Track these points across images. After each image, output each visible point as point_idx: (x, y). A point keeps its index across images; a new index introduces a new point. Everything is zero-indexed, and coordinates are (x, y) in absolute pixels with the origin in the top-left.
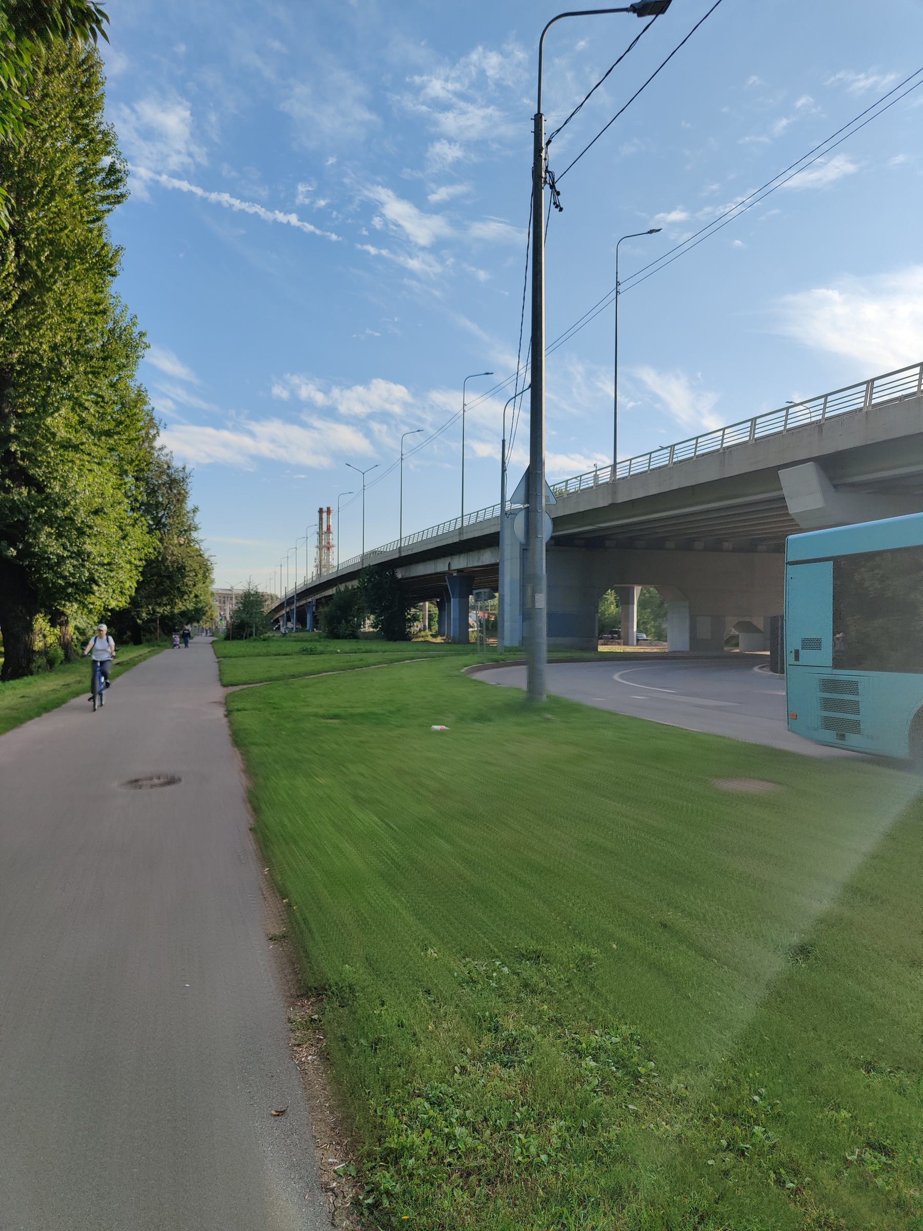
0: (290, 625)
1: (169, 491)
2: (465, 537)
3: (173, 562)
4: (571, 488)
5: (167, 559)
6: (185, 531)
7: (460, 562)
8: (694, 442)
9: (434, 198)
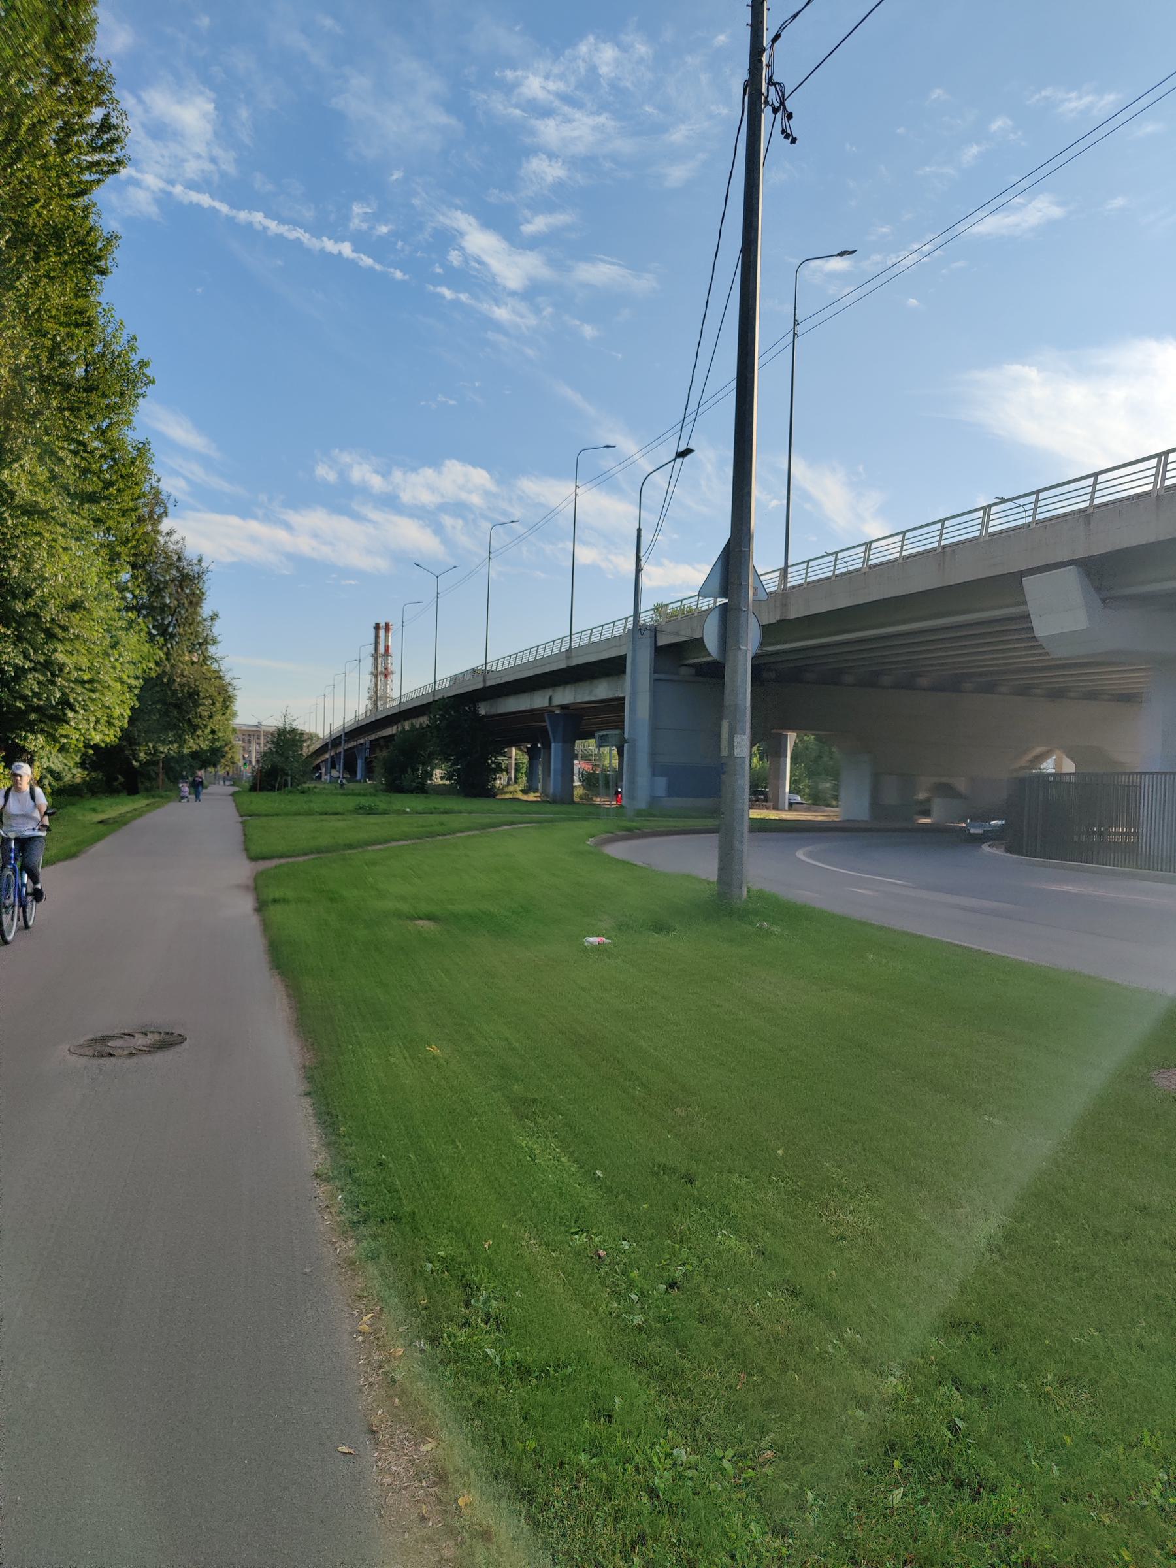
0: (335, 773)
1: (179, 590)
2: (575, 662)
3: (182, 686)
4: (704, 604)
5: (174, 681)
6: (200, 644)
7: (565, 696)
8: (1090, 481)
9: (528, 229)
